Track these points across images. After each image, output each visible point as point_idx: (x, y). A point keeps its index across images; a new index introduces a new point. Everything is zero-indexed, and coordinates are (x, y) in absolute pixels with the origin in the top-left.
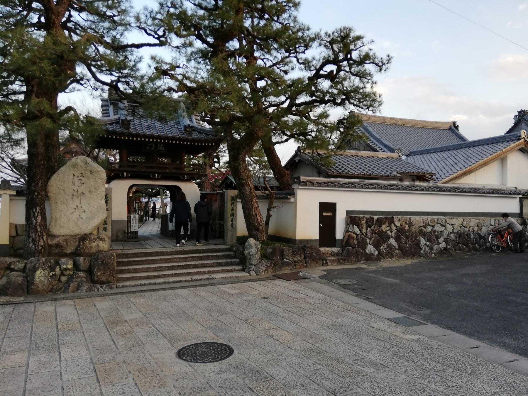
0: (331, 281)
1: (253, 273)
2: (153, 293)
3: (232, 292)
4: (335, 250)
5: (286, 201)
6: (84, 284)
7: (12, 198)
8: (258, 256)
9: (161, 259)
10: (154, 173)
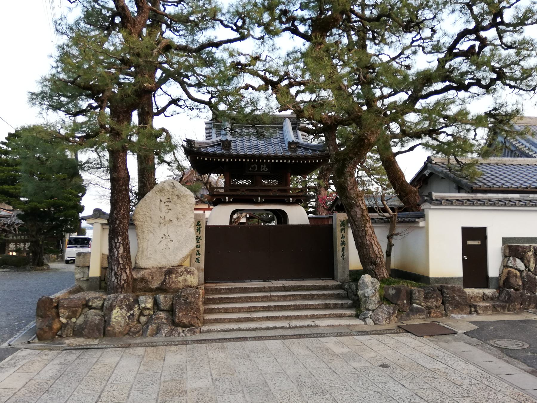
0: (486, 341)
1: (370, 321)
2: (238, 344)
3: (338, 350)
4: (489, 292)
5: (412, 225)
6: (164, 326)
7: (105, 227)
8: (376, 299)
9: (256, 297)
10: (257, 196)
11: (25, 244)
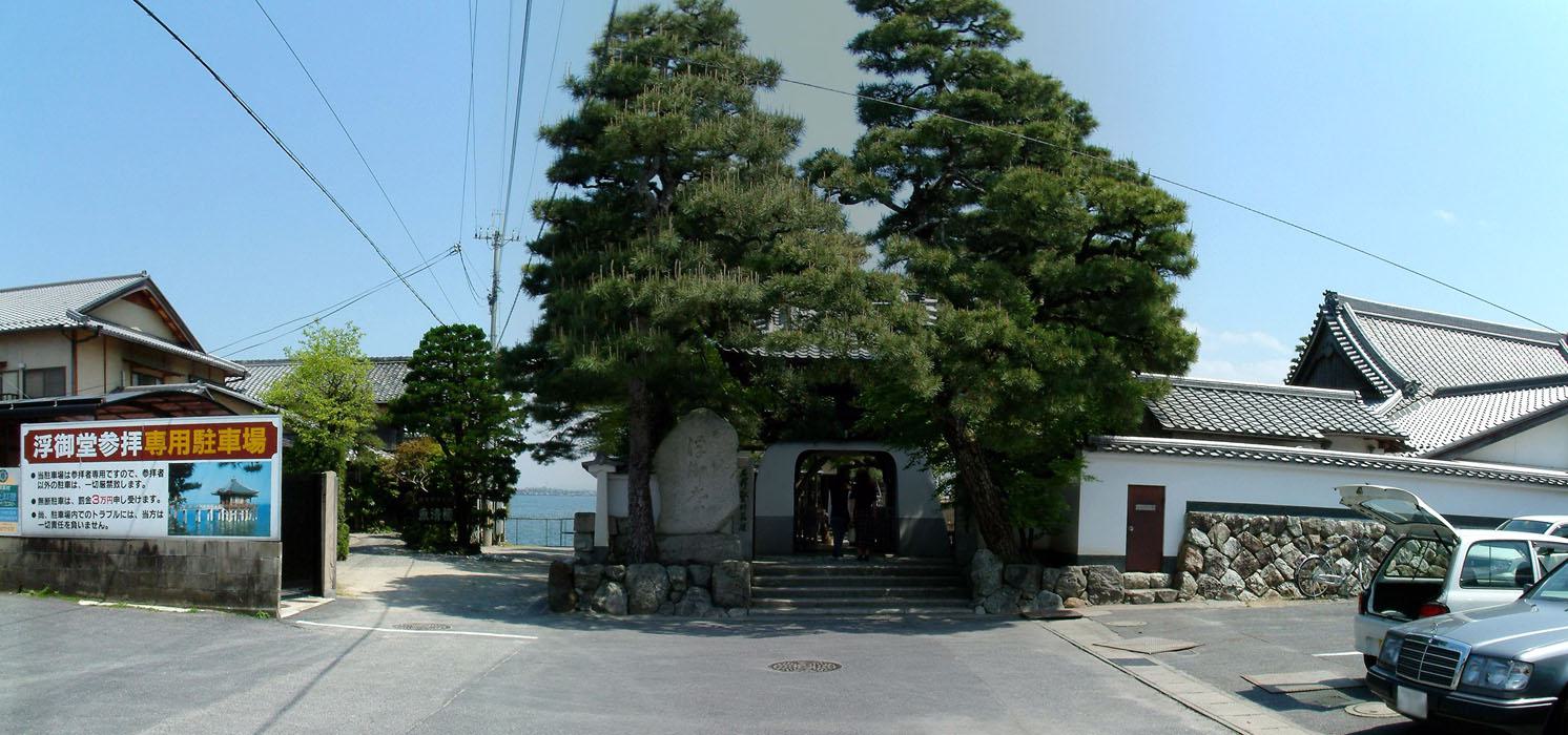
11: (442, 511)
